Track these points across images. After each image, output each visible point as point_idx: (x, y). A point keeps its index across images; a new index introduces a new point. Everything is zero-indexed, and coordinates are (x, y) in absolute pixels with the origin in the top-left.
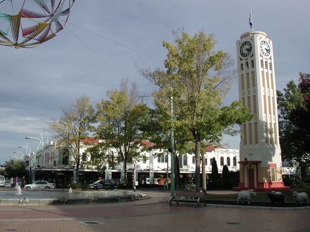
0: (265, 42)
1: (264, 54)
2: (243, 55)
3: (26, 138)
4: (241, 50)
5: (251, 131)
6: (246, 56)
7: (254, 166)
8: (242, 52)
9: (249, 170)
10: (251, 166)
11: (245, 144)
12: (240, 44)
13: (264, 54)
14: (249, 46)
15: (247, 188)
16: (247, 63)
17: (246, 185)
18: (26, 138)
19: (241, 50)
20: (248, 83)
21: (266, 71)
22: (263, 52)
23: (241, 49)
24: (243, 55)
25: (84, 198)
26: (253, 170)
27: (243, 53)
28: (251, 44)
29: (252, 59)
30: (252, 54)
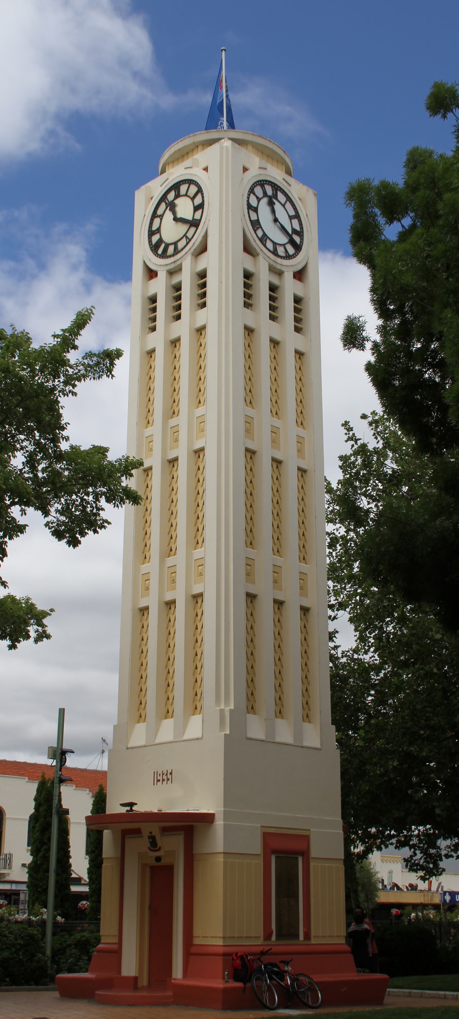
0: (262, 186)
1: (270, 245)
2: (160, 251)
3: (62, 712)
4: (154, 228)
5: (167, 646)
6: (176, 251)
7: (173, 845)
8: (155, 238)
9: (152, 868)
10: (159, 844)
11: (252, 709)
12: (152, 198)
13: (270, 245)
14: (193, 199)
15: (135, 979)
16: (178, 288)
17: (130, 965)
18: (62, 712)
19: (154, 228)
20: (173, 391)
21: (266, 329)
22: (260, 233)
23: (157, 221)
24: (160, 251)
25: (19, 920)
26: (170, 870)
27: (160, 241)
28: (200, 190)
29: (200, 268)
30: (200, 239)
